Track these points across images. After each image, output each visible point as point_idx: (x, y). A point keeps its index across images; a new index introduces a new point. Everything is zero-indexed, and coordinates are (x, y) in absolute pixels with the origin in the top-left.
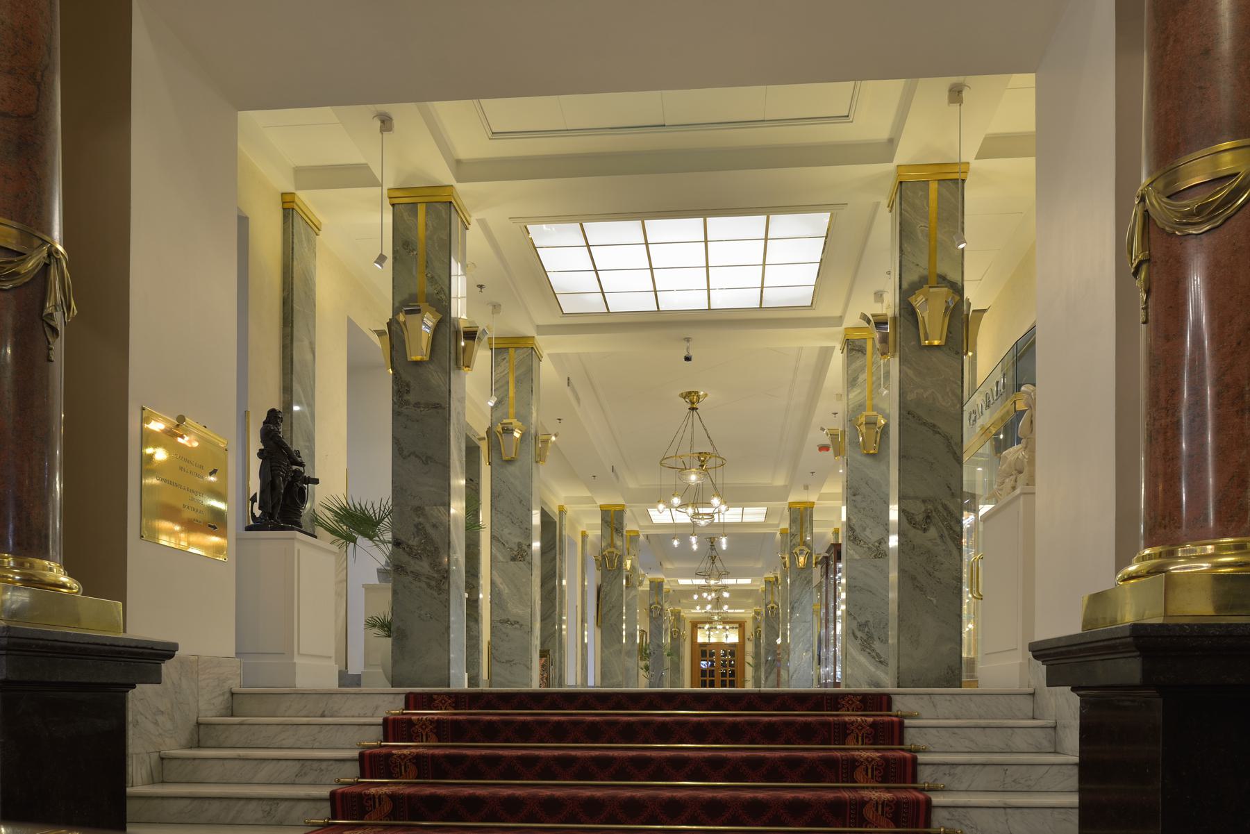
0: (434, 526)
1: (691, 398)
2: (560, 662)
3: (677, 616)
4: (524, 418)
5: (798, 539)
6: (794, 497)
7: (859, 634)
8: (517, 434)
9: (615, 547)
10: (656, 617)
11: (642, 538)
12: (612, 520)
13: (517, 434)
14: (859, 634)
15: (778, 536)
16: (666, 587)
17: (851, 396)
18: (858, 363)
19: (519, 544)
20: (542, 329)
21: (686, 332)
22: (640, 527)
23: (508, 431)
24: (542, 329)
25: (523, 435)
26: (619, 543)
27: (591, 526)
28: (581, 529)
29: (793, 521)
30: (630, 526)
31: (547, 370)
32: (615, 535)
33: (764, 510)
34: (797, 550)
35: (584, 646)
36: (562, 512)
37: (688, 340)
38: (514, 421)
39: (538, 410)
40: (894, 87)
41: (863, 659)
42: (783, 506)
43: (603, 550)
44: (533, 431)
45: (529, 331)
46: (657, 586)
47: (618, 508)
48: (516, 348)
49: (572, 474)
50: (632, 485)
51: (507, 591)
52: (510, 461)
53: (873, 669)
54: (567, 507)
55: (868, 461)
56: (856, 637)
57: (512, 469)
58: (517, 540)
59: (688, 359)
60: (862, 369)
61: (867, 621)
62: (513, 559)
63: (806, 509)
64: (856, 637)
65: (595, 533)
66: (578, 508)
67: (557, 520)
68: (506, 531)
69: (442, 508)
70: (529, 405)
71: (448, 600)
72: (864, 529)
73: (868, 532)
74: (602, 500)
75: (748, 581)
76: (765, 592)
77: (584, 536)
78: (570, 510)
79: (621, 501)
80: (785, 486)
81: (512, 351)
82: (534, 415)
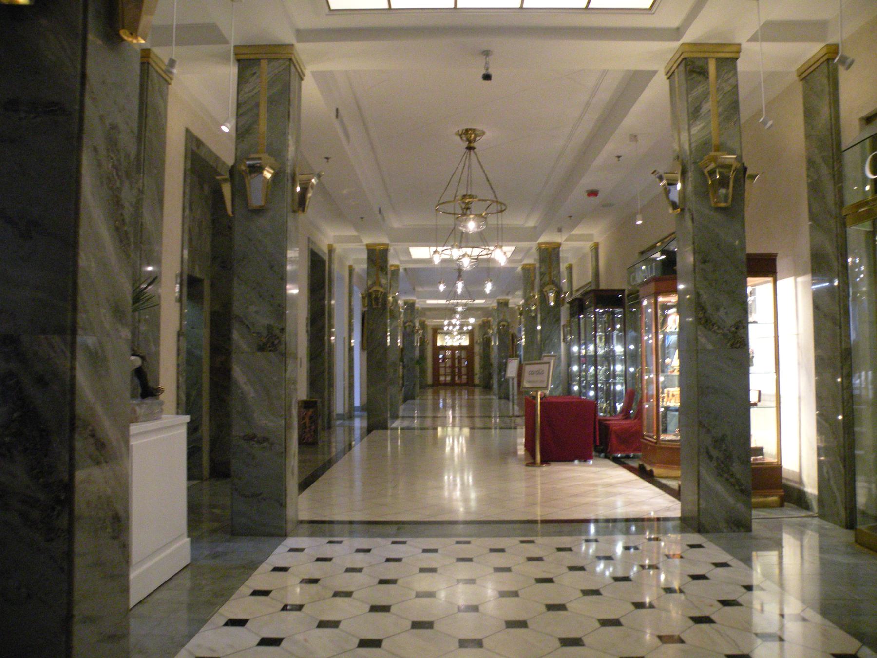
0: (41, 381)
1: (469, 137)
2: (330, 400)
3: (423, 325)
4: (277, 153)
5: (547, 278)
6: (543, 239)
7: (715, 453)
8: (268, 174)
9: (381, 285)
10: (408, 336)
11: (401, 270)
12: (378, 258)
13: (268, 174)
14: (715, 453)
15: (520, 268)
16: (417, 305)
17: (694, 130)
18: (699, 90)
19: (269, 328)
20: (304, 35)
21: (484, 42)
22: (401, 261)
23: (257, 169)
24: (304, 35)
25: (275, 176)
26: (384, 281)
27: (359, 260)
28: (348, 264)
29: (542, 260)
30: (392, 261)
31: (309, 91)
32: (380, 273)
33: (512, 248)
34: (546, 289)
35: (351, 349)
36: (331, 250)
37: (486, 53)
38: (265, 156)
39: (297, 142)
40: (236, 281)
41: (719, 488)
42: (534, 245)
43: (369, 289)
44: (289, 170)
45: (286, 37)
46: (410, 306)
47: (382, 247)
48: (270, 60)
49: (339, 215)
50: (396, 224)
51: (252, 395)
52: (259, 211)
53: (731, 500)
54: (335, 245)
55: (718, 217)
56: (711, 457)
57: (262, 221)
58: (266, 322)
59: (487, 77)
60: (706, 95)
61: (724, 436)
62: (261, 348)
63: (554, 249)
64: (711, 457)
65: (361, 265)
66: (347, 246)
67: (326, 258)
68: (253, 309)
69: (56, 339)
70: (284, 134)
71: (69, 555)
72: (717, 309)
73: (722, 313)
74: (368, 240)
75: (482, 301)
76: (498, 310)
77: (351, 270)
78: (339, 248)
79: (385, 240)
80: (535, 227)
81: (264, 63)
82: (292, 149)
